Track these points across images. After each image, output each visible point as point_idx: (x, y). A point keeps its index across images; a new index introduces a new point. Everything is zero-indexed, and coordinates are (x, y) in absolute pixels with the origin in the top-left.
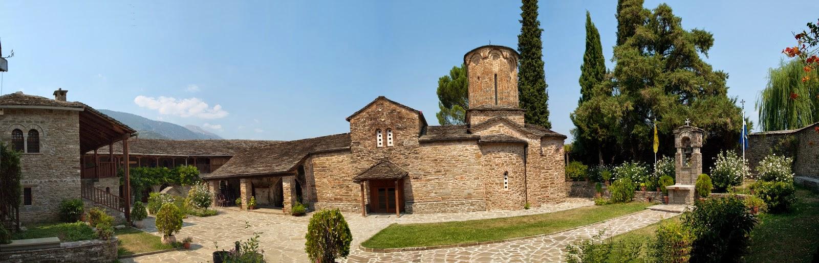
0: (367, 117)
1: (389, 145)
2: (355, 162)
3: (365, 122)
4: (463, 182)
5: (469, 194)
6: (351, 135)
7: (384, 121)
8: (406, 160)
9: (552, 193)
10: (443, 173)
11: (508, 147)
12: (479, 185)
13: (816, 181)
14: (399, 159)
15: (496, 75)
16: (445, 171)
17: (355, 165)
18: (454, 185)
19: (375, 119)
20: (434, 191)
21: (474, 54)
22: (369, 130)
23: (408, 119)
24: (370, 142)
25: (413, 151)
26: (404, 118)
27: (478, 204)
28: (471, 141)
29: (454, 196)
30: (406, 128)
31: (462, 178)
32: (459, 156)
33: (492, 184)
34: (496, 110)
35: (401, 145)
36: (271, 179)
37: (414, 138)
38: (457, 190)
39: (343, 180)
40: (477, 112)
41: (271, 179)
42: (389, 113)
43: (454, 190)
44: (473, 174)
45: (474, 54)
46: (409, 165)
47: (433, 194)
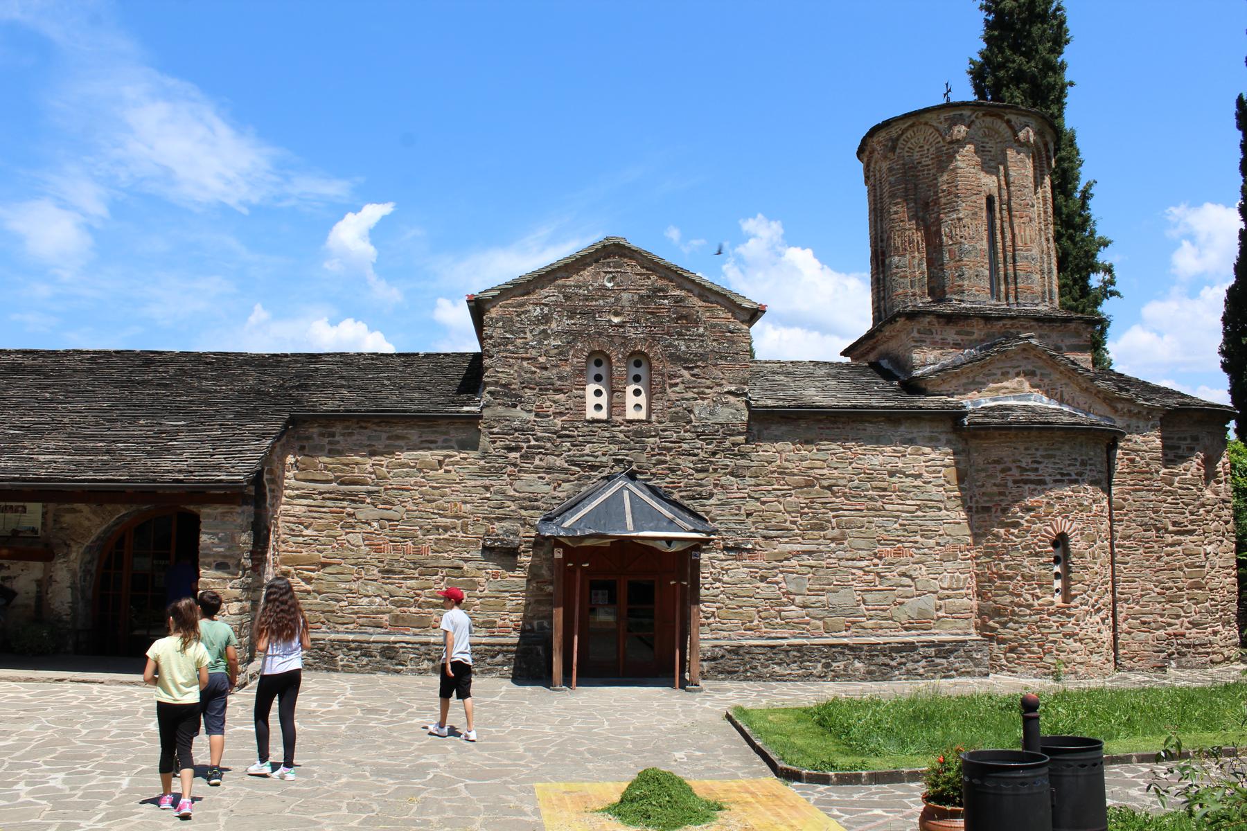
0: (557, 304)
1: (631, 414)
2: (499, 471)
3: (546, 319)
4: (903, 569)
5: (922, 613)
6: (487, 362)
7: (622, 325)
8: (701, 475)
9: (1195, 624)
10: (830, 533)
11: (1067, 448)
12: (958, 580)
13: (3, 504)
14: (672, 470)
15: (990, 200)
16: (839, 526)
17: (496, 483)
18: (870, 577)
19: (589, 314)
20: (798, 599)
21: (911, 126)
22: (562, 353)
23: (713, 326)
24: (561, 397)
25: (727, 444)
26: (696, 323)
27: (961, 653)
28: (931, 420)
29: (871, 618)
30: (703, 357)
31: (898, 553)
32: (892, 474)
33: (1010, 578)
34: (1000, 318)
35: (681, 418)
36: (68, 519)
37: (732, 399)
38: (878, 596)
39: (437, 541)
40: (935, 321)
41: (68, 519)
42: (641, 297)
43: (868, 597)
44: (938, 539)
45: (911, 126)
46: (711, 495)
47: (793, 611)
